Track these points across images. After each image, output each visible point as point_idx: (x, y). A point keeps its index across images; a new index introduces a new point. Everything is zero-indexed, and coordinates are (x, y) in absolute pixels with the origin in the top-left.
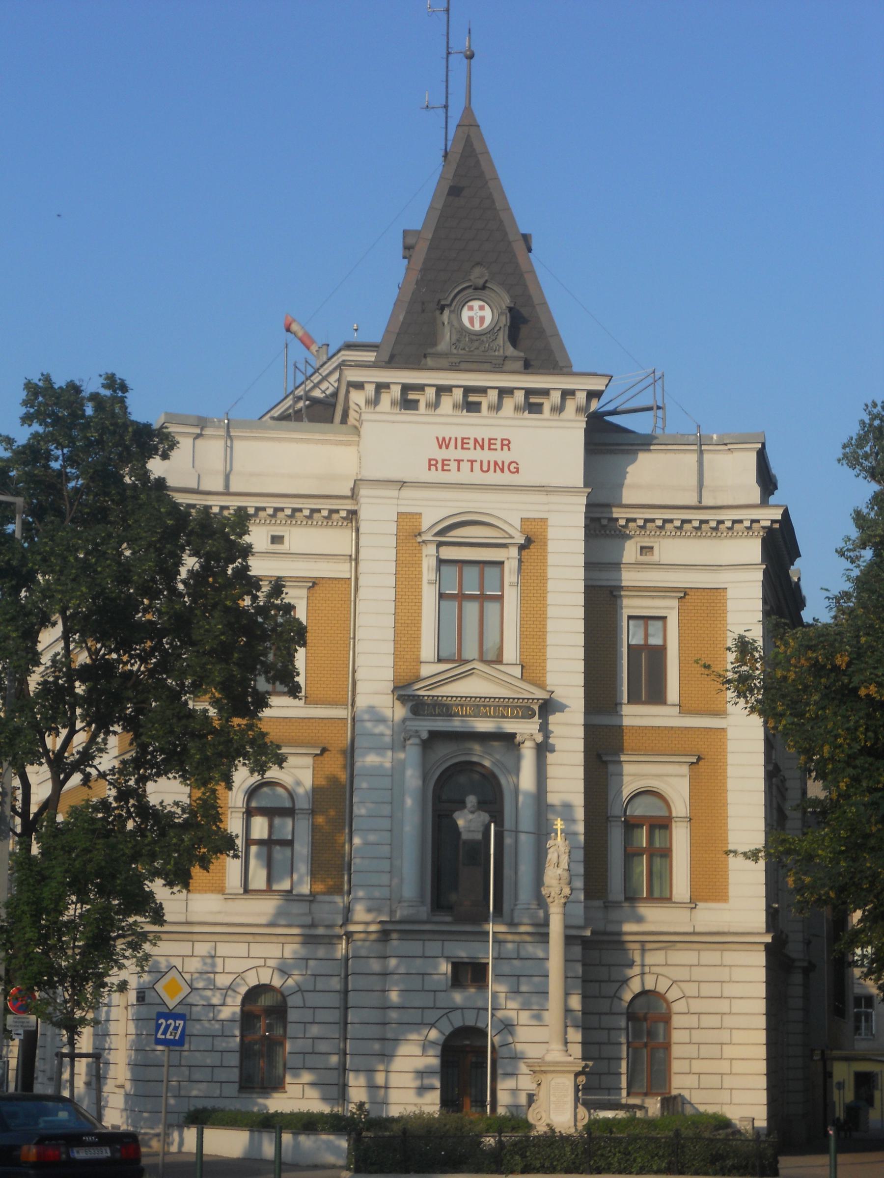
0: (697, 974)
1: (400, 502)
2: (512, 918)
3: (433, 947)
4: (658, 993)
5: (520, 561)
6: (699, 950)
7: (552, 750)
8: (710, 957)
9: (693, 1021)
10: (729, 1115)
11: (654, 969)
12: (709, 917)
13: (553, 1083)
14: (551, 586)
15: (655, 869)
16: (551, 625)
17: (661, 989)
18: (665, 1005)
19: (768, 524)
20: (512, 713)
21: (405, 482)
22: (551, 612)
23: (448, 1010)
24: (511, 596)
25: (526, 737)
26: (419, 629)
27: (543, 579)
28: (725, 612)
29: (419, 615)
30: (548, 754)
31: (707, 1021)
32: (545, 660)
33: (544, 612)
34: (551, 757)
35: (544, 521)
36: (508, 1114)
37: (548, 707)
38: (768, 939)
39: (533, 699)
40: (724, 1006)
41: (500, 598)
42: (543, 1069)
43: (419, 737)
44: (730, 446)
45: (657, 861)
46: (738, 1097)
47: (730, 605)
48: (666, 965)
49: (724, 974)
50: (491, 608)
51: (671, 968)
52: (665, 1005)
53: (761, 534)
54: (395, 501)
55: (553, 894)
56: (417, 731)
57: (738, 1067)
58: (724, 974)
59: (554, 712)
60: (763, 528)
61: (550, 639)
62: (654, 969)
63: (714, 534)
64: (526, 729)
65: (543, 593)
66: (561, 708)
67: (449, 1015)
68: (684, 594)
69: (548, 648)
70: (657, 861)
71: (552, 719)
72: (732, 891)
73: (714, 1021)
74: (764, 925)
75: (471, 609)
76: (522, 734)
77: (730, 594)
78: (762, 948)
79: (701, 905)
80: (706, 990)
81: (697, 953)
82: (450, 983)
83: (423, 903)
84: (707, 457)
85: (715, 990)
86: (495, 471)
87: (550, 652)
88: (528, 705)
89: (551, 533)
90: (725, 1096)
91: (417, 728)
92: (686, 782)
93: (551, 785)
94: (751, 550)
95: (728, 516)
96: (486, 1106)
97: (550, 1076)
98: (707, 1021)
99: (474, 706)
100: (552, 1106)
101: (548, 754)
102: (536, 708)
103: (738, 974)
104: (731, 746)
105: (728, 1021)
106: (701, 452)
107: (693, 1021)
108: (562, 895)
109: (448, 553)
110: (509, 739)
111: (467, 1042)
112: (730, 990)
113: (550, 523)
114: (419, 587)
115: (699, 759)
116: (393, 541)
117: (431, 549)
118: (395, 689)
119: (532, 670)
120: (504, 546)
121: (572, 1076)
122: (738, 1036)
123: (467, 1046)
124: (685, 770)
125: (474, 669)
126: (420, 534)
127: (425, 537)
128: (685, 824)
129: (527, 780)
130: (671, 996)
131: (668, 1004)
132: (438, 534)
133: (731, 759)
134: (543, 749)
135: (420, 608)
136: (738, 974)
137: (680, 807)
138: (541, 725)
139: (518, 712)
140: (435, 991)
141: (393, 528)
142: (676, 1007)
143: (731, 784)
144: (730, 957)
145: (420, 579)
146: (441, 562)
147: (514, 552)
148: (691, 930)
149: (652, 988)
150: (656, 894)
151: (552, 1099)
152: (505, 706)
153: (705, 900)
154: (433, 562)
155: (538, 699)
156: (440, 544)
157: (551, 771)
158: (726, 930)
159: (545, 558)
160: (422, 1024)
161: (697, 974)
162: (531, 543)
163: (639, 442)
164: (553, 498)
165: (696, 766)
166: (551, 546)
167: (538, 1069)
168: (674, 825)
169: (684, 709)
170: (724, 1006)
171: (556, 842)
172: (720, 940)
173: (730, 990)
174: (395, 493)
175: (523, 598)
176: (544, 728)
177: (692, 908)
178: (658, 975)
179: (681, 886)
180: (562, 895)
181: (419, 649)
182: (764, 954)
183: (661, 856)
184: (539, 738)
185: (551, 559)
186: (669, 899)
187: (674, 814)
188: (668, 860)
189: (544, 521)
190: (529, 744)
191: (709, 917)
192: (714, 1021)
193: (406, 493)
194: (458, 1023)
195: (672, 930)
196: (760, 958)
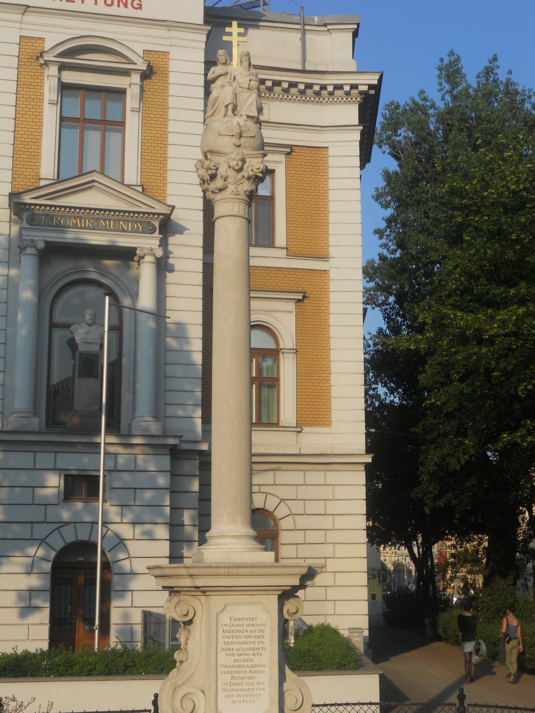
0: (303, 492)
1: (23, 26)
2: (130, 430)
3: (45, 459)
4: (267, 511)
5: (142, 90)
6: (304, 471)
7: (172, 270)
8: (315, 476)
9: (298, 537)
10: (334, 622)
11: (263, 489)
12: (314, 440)
13: (225, 619)
14: (172, 114)
15: (263, 398)
16: (171, 151)
17: (270, 507)
18: (272, 523)
19: (366, 88)
20: (133, 227)
21: (28, 7)
22: (172, 138)
23: (64, 524)
24: (133, 123)
25: (146, 251)
26: (39, 147)
27: (164, 108)
28: (327, 168)
29: (40, 134)
30: (168, 274)
31: (312, 537)
32: (165, 185)
33: (165, 139)
34: (170, 277)
35: (166, 54)
36: (119, 647)
37: (167, 226)
38: (368, 459)
39: (154, 214)
40: (327, 522)
41: (122, 124)
42: (200, 582)
43: (35, 247)
44: (329, 27)
45: (265, 391)
46: (341, 608)
47: (332, 162)
48: (275, 485)
49: (327, 493)
50: (113, 138)
51: (278, 487)
52: (272, 523)
53: (359, 99)
54: (18, 25)
55: (222, 171)
56: (33, 241)
57: (341, 579)
58: (327, 493)
59: (173, 234)
60: (361, 93)
61: (171, 164)
62: (263, 489)
63: (317, 99)
64: (147, 243)
65: (164, 120)
66: (181, 230)
67: (61, 530)
68: (290, 150)
69: (169, 173)
70: (265, 391)
71: (171, 240)
72: (335, 416)
73: (319, 536)
74: (364, 447)
75: (93, 137)
76: (142, 248)
77: (331, 152)
78: (362, 468)
79: (306, 429)
80: (311, 507)
81: (302, 473)
82: (62, 497)
83: (36, 414)
84: (308, 36)
85: (319, 507)
86: (119, 6)
87: (171, 176)
88: (149, 220)
89: (173, 66)
90: (329, 607)
91: (34, 238)
92: (292, 318)
93: (170, 303)
94: (350, 113)
95: (330, 80)
96: (94, 631)
97: (216, 601)
98: (312, 537)
99: (93, 219)
100: (223, 679)
101: (168, 274)
102: (157, 224)
103: (341, 493)
104: (333, 286)
105: (332, 537)
106: (304, 32)
107: (298, 537)
108: (245, 173)
109: (70, 77)
110: (127, 255)
111: (82, 559)
112: (333, 507)
113: (171, 56)
114: (41, 107)
115: (304, 297)
116: (14, 62)
117: (53, 70)
118: (11, 195)
119: (152, 184)
120: (126, 73)
121: (273, 601)
122: (341, 551)
123: (82, 561)
124: (291, 306)
125: (94, 181)
126: (41, 55)
127: (46, 58)
128: (292, 355)
129: (146, 299)
130: (279, 514)
131: (276, 521)
132: (62, 55)
133: (333, 297)
134: (163, 266)
135: (40, 127)
136: (341, 493)
137: (288, 339)
138: (161, 241)
139: (138, 227)
140: (46, 505)
141: (15, 50)
142: (284, 524)
143: (333, 320)
144: (333, 477)
145: (42, 100)
146: (65, 88)
147: (136, 78)
148: (297, 452)
149: (261, 506)
150: (264, 420)
151: (224, 659)
152: (125, 221)
153: (310, 425)
154: (54, 82)
155: (159, 214)
156: (63, 67)
157: (170, 290)
158: (329, 452)
159: (166, 88)
160: (31, 539)
161: (303, 492)
162: (151, 73)
163: (250, 17)
164: (174, 33)
165: (302, 304)
166: (172, 78)
167: (187, 582)
168: (281, 356)
169: (291, 252)
170: (327, 522)
171: (229, 69)
172: (323, 462)
173: (333, 507)
174: (18, 17)
175: (145, 125)
176: (164, 243)
177: (298, 432)
178: (267, 493)
179: (288, 412)
180: (245, 173)
181: (38, 167)
182: (364, 473)
183: (269, 387)
184: (160, 253)
185: (172, 90)
186: (277, 425)
187: (281, 346)
188: (275, 391)
189: (166, 54)
190: (148, 258)
191: (314, 440)
192: (319, 536)
193: (29, 18)
194: (70, 538)
195: (280, 452)
196: (361, 477)
